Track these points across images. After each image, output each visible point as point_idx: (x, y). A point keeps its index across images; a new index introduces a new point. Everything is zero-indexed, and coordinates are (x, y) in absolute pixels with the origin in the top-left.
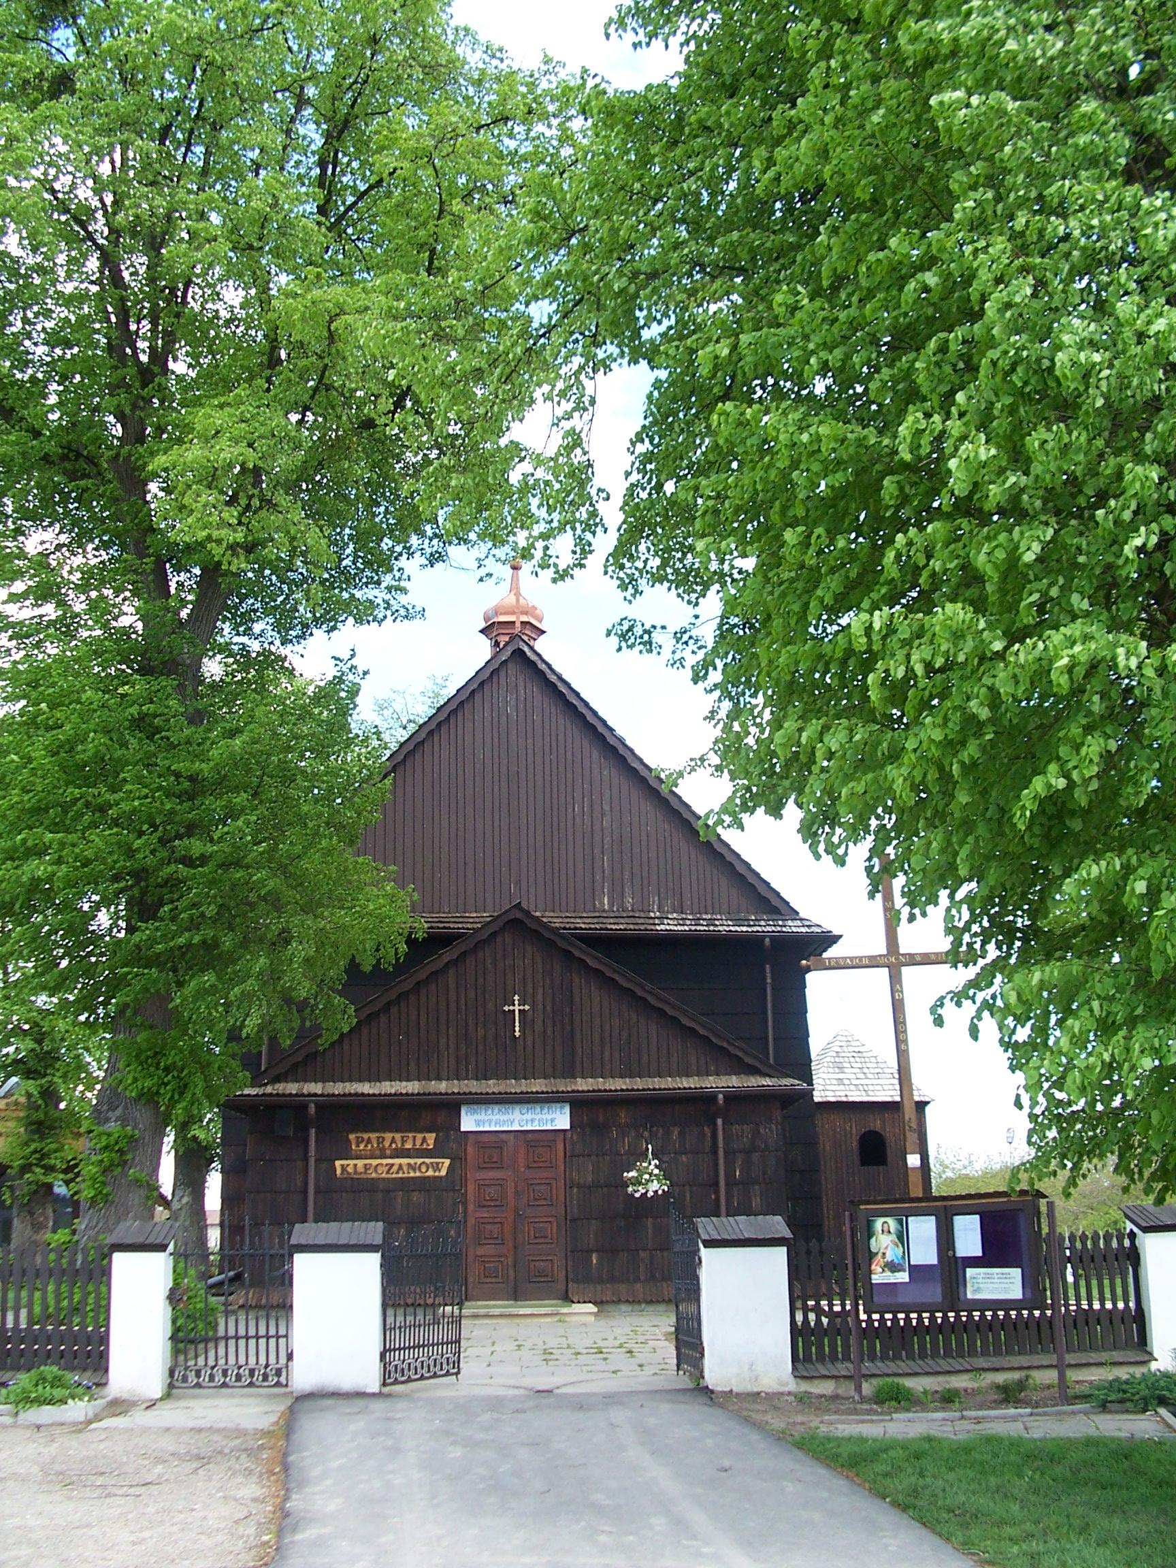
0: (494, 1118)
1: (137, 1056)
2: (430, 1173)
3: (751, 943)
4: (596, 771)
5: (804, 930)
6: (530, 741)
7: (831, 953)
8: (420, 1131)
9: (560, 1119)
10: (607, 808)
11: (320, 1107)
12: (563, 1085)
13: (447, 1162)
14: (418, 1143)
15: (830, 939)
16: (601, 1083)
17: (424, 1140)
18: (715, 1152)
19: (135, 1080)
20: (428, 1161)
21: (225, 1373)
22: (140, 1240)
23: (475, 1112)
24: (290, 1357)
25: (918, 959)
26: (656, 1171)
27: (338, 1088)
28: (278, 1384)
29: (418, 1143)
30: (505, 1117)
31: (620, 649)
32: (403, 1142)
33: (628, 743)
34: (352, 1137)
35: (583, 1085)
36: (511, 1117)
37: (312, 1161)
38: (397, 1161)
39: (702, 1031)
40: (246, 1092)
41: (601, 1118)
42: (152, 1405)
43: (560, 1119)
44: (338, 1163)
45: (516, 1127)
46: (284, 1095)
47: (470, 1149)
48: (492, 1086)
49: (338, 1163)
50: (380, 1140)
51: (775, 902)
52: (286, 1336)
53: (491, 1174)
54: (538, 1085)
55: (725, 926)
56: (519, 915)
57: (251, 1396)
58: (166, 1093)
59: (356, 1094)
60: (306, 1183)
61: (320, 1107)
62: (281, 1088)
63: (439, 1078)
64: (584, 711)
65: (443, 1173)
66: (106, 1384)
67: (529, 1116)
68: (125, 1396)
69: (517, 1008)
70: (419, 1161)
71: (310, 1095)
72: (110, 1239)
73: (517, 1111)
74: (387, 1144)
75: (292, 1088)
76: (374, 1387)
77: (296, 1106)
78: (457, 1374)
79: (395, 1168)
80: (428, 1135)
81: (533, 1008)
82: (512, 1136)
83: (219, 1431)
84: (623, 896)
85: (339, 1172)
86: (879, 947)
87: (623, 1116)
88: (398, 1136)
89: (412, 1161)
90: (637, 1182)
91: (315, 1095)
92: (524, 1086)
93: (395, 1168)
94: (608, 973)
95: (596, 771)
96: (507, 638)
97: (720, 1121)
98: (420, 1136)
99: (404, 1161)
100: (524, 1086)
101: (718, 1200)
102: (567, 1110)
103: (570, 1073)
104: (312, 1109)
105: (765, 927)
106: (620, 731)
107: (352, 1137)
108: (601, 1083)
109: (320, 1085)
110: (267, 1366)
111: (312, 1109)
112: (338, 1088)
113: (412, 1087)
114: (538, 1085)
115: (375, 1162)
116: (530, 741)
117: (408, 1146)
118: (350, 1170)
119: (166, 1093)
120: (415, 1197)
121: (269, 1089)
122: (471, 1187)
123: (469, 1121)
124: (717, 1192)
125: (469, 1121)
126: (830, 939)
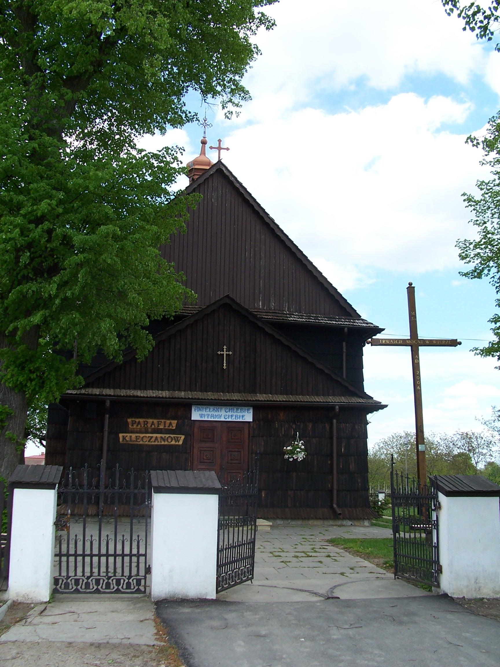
0: (210, 413)
1: (15, 362)
2: (173, 443)
3: (339, 329)
4: (258, 236)
5: (365, 325)
6: (223, 217)
7: (378, 336)
8: (168, 419)
9: (248, 416)
10: (263, 255)
11: (112, 402)
12: (250, 397)
13: (183, 437)
14: (167, 425)
15: (379, 330)
16: (270, 397)
17: (170, 424)
18: (331, 438)
19: (13, 376)
20: (172, 436)
21: (98, 582)
22: (36, 479)
23: (200, 410)
24: (148, 570)
25: (435, 342)
26: (303, 447)
27: (123, 392)
28: (138, 591)
29: (167, 425)
30: (217, 413)
31: (464, 29)
32: (158, 425)
33: (276, 221)
34: (129, 420)
35: (261, 397)
36: (220, 413)
37: (106, 433)
38: (155, 435)
39: (326, 371)
40: (69, 392)
41: (270, 416)
42: (44, 608)
43: (248, 416)
44: (121, 435)
45: (222, 419)
46: (92, 395)
47: (196, 430)
48: (210, 395)
49: (121, 435)
50: (146, 423)
51: (348, 310)
52: (145, 555)
53: (207, 445)
54: (236, 396)
55: (324, 321)
56: (228, 301)
57: (118, 599)
58: (31, 386)
59: (134, 396)
60: (102, 445)
61: (112, 402)
62: (90, 391)
63: (180, 390)
64: (253, 204)
65: (181, 443)
66: (6, 590)
67: (230, 413)
68: (20, 599)
69: (225, 353)
70: (167, 436)
71: (106, 395)
72: (14, 478)
73: (223, 411)
74: (149, 425)
75: (97, 391)
76: (213, 595)
77: (99, 401)
78: (252, 578)
79: (153, 439)
80: (173, 421)
81: (234, 354)
82: (220, 423)
83: (115, 647)
84: (269, 302)
85: (121, 440)
86: (406, 335)
87: (282, 416)
88: (155, 421)
89: (163, 436)
90: (292, 452)
91: (110, 395)
92: (227, 396)
93: (153, 439)
94: (277, 336)
95: (258, 236)
96: (198, 176)
97: (335, 421)
98: (168, 422)
99: (159, 435)
100: (227, 396)
101: (332, 465)
102: (251, 411)
103: (254, 391)
104: (108, 404)
105: (344, 322)
106: (272, 215)
107: (129, 420)
108: (270, 397)
109: (112, 390)
110: (130, 577)
111: (108, 404)
112: (123, 392)
113: (165, 394)
114: (236, 396)
115: (142, 435)
116: (223, 217)
117: (161, 427)
118: (127, 439)
119: (31, 386)
120: (164, 455)
121: (83, 391)
122: (196, 451)
123: (196, 415)
124: (332, 460)
125: (196, 415)
126: (379, 330)
